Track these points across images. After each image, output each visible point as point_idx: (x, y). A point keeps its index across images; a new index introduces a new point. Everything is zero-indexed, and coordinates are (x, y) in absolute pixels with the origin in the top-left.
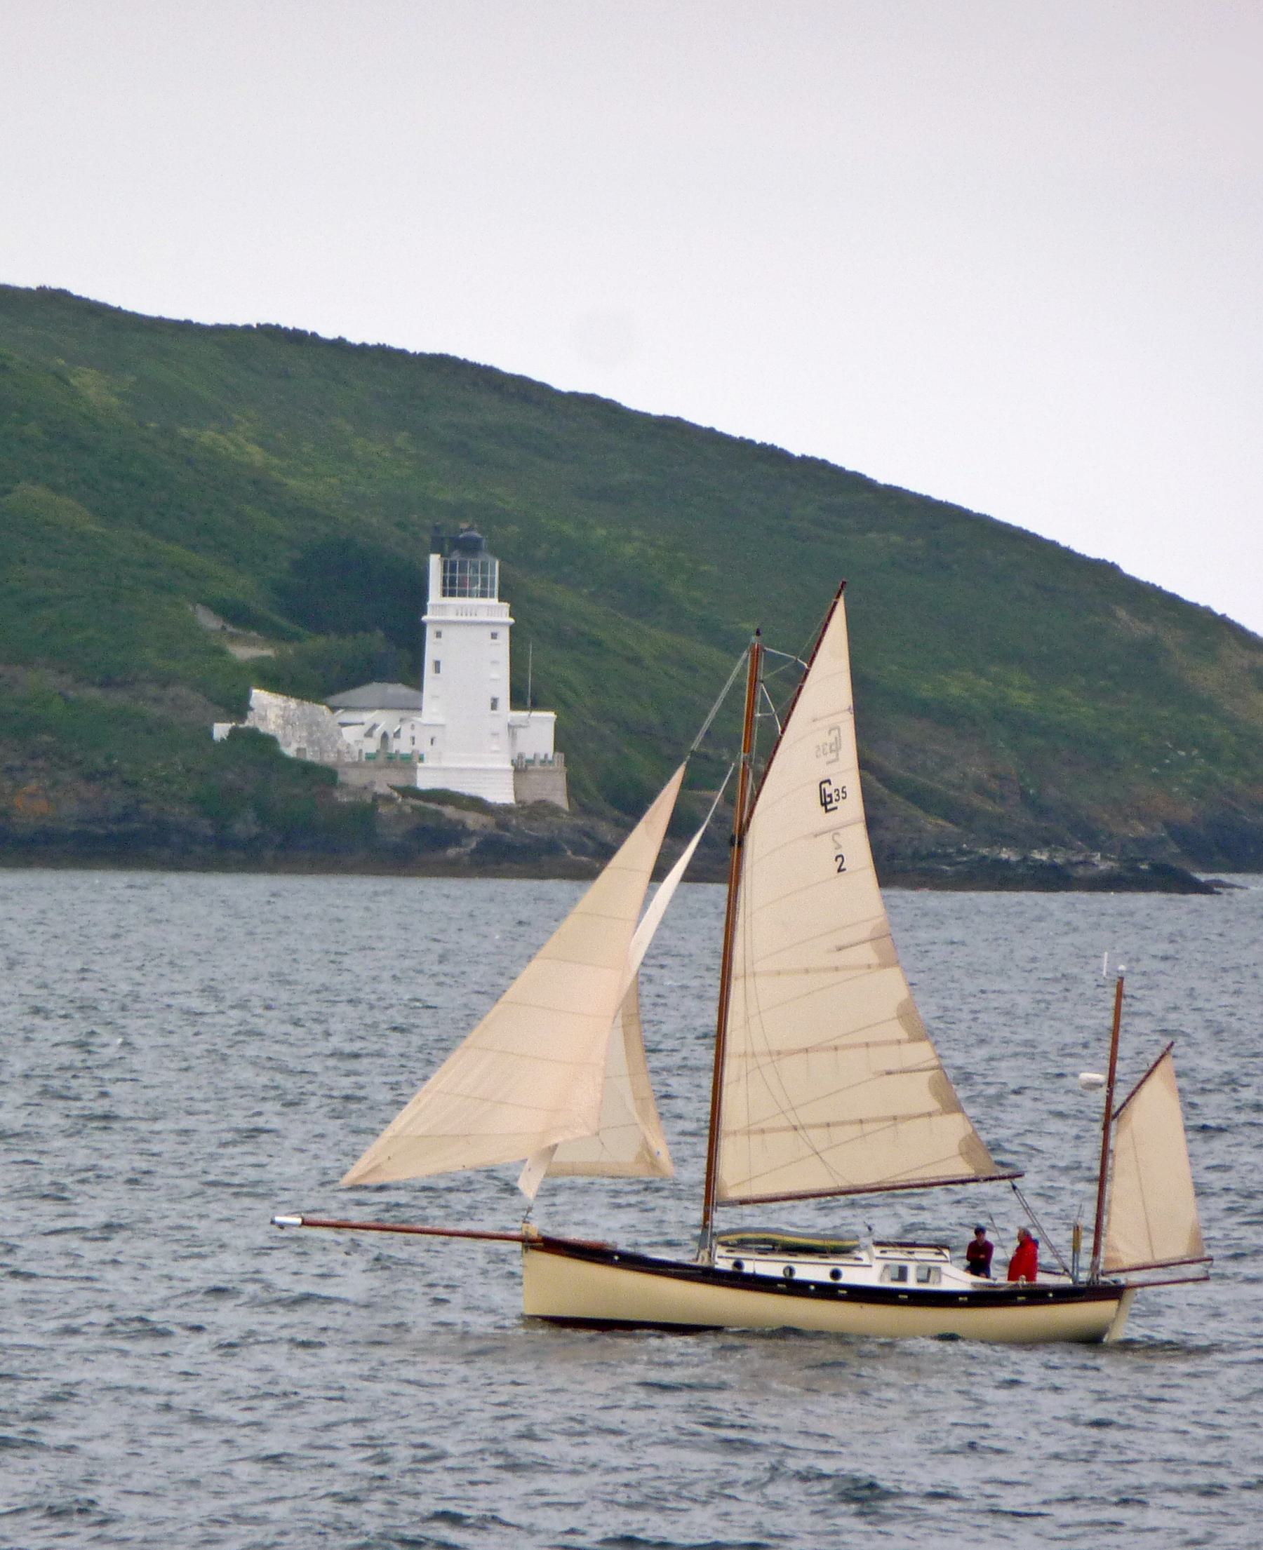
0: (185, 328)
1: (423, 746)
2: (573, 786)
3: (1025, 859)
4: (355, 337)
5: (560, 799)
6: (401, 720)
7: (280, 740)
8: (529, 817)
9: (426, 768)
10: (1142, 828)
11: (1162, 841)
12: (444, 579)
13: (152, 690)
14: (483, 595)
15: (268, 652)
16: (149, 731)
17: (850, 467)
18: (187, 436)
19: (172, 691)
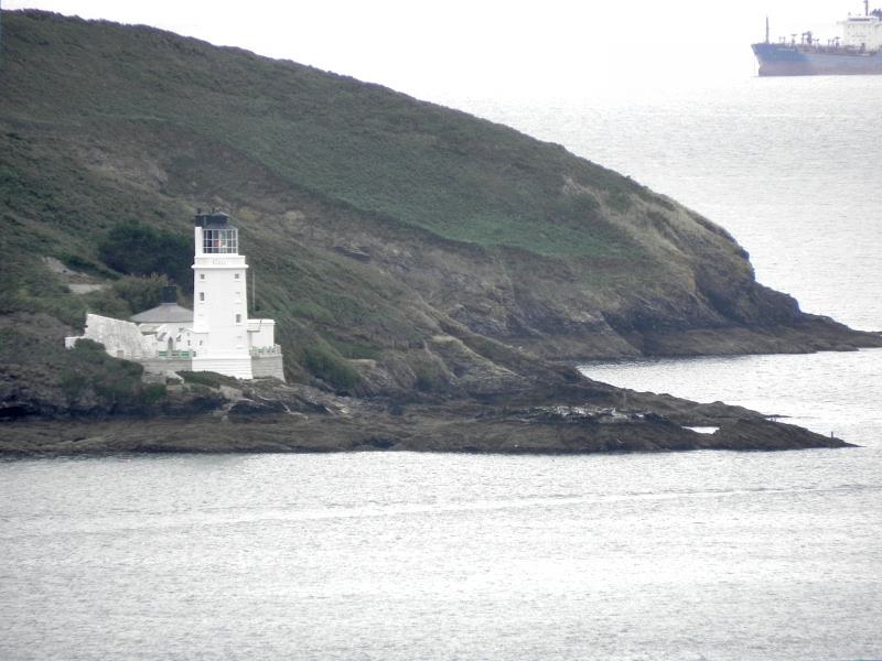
1: (195, 347)
5: (280, 375)
6: (181, 330)
9: (198, 360)
10: (589, 316)
11: (601, 323)
13: (25, 316)
14: (229, 251)
19: (37, 317)
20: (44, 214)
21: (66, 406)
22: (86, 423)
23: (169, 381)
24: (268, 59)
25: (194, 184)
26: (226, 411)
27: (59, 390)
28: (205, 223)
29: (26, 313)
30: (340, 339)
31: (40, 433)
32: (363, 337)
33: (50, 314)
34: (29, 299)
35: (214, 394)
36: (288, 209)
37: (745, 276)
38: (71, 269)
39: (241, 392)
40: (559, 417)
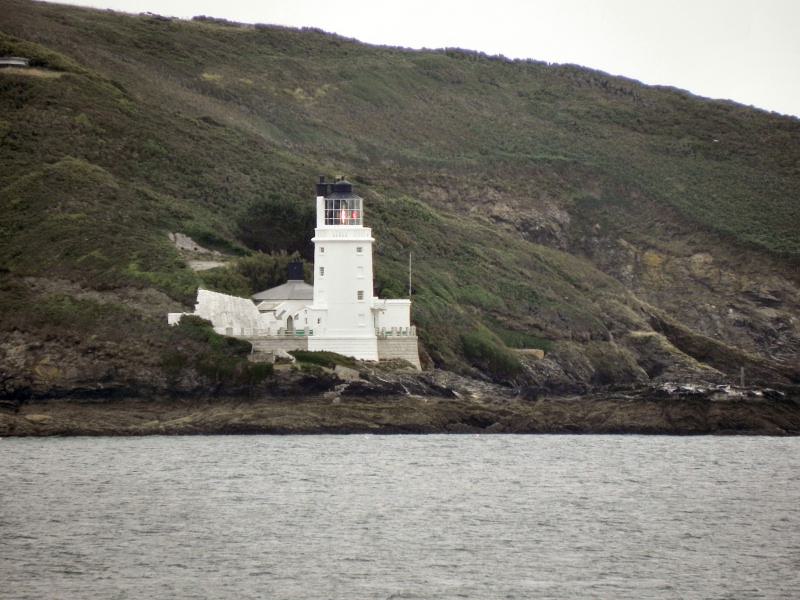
3: (678, 390)
4: (511, 55)
5: (414, 360)
12: (326, 212)
13: (132, 292)
14: (352, 222)
19: (145, 293)
20: (189, 191)
21: (165, 386)
22: (186, 405)
23: (279, 360)
24: (704, 99)
25: (598, 226)
26: (339, 393)
27: (159, 370)
28: (329, 190)
29: (134, 289)
30: (511, 328)
31: (136, 416)
32: (536, 326)
33: (160, 289)
34: (137, 273)
35: (327, 374)
36: (696, 252)
38: (202, 246)
39: (358, 373)
40: (666, 393)
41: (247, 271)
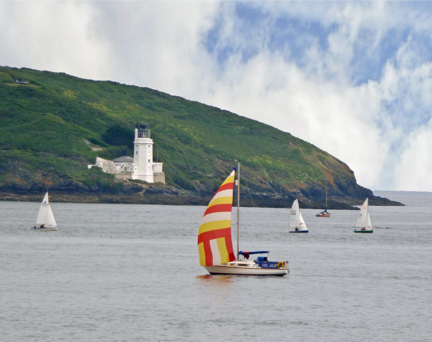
0: (91, 81)
2: (166, 179)
5: (164, 182)
7: (103, 168)
8: (157, 186)
11: (299, 192)
14: (147, 137)
15: (101, 149)
16: (74, 166)
17: (233, 112)
18: (268, 157)
19: (79, 158)
37: (352, 179)
41: (111, 152)
